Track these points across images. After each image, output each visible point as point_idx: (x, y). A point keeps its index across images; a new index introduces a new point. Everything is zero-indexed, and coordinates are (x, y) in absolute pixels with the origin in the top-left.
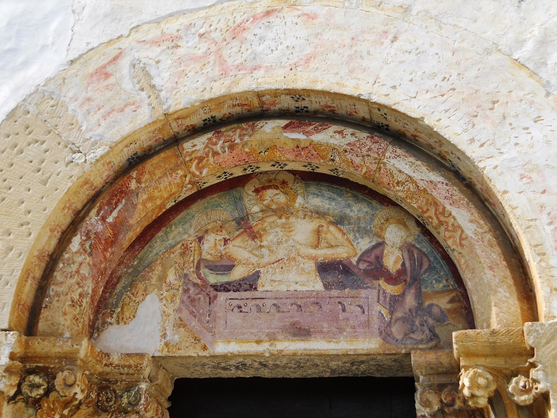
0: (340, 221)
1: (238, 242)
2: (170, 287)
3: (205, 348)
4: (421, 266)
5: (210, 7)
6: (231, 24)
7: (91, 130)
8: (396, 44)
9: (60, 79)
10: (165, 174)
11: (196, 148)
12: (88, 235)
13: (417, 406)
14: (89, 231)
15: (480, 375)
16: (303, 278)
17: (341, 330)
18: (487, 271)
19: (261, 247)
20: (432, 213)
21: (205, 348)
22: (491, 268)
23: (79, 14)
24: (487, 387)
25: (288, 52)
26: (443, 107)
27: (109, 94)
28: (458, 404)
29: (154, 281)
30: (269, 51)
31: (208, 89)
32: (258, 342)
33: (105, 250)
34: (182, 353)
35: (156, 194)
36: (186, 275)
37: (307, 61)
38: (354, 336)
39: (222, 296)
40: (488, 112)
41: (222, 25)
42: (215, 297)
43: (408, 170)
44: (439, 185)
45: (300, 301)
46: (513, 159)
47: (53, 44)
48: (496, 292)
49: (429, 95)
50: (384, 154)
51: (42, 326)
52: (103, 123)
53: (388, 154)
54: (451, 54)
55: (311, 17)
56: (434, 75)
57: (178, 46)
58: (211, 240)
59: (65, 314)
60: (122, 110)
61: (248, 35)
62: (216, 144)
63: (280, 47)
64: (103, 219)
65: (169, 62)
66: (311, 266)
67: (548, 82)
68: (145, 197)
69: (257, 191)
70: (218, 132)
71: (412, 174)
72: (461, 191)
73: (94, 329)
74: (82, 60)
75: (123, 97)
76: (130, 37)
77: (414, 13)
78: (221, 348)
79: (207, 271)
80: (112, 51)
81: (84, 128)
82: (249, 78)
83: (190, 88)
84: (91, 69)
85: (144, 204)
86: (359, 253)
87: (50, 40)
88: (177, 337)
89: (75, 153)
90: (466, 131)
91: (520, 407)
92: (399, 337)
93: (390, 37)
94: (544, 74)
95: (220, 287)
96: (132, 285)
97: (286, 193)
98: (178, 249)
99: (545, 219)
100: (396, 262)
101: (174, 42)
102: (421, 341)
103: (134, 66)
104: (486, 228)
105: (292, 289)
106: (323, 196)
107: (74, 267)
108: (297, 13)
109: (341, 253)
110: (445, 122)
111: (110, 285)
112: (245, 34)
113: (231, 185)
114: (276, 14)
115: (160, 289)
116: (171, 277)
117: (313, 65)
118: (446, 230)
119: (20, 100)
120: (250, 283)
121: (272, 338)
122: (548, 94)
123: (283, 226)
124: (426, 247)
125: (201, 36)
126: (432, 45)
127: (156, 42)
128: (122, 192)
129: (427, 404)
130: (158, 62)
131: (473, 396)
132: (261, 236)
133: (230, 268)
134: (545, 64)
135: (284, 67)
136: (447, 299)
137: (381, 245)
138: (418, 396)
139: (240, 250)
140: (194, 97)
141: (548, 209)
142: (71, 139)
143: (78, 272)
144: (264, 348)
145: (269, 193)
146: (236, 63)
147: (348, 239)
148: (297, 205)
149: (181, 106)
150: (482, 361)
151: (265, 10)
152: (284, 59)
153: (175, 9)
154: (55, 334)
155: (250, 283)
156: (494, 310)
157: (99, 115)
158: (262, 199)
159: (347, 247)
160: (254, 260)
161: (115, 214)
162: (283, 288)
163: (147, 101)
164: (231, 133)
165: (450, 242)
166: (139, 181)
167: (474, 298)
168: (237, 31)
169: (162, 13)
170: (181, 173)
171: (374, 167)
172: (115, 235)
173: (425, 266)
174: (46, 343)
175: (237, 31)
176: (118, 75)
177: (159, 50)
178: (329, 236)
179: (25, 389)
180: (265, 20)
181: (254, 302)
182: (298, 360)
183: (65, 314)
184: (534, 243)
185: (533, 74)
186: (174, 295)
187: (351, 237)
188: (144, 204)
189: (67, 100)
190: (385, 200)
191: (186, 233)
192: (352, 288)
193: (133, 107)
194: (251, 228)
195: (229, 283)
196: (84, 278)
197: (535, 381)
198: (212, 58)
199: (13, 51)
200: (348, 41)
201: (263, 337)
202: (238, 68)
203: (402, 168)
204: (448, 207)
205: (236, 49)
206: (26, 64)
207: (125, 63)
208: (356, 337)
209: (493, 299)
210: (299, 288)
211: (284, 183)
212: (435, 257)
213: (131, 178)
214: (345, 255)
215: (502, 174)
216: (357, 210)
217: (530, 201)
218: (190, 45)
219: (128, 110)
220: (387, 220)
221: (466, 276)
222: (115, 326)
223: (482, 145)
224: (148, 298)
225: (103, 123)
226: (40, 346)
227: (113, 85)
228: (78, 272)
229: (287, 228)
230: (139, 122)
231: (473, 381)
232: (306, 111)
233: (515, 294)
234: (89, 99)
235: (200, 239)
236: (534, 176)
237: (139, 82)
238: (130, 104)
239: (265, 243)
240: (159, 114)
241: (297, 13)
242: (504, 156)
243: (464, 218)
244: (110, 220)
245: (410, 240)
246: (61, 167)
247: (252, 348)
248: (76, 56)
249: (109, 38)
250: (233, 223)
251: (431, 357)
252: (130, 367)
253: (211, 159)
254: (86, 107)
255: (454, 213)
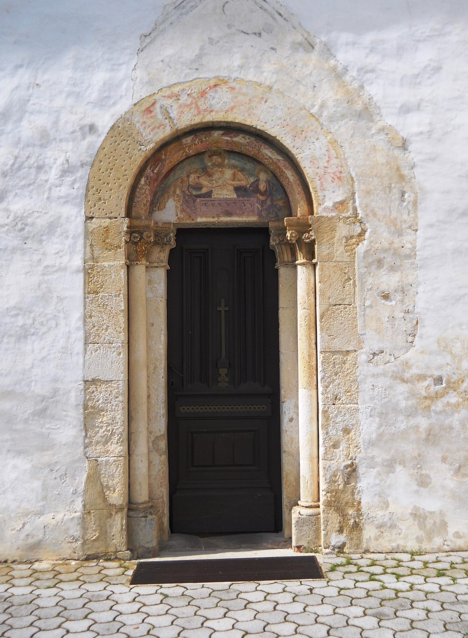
0: (242, 170)
1: (203, 178)
2: (178, 196)
3: (193, 220)
4: (273, 189)
5: (191, 81)
6: (200, 90)
7: (147, 136)
8: (267, 103)
9: (130, 112)
10: (176, 153)
11: (188, 142)
12: (147, 177)
13: (271, 241)
14: (148, 176)
15: (293, 233)
16: (229, 193)
17: (243, 213)
18: (297, 195)
19: (212, 180)
20: (278, 171)
21: (193, 220)
22: (298, 194)
23: (135, 81)
24: (296, 237)
25: (224, 105)
26: (284, 132)
27: (152, 120)
28: (285, 241)
29: (171, 193)
30: (216, 104)
31: (193, 120)
32: (213, 217)
33: (154, 183)
34: (184, 222)
35: (173, 160)
36: (184, 191)
37: (232, 109)
38: (248, 216)
39: (198, 200)
40: (300, 135)
41: (196, 90)
42: (196, 200)
43: (269, 154)
44: (281, 161)
45: (227, 201)
46: (308, 155)
47: (125, 95)
48: (300, 203)
49: (279, 127)
50: (260, 147)
51: (133, 214)
52: (151, 133)
53: (262, 148)
54: (287, 109)
55: (233, 89)
56: (280, 118)
57: (179, 99)
58: (192, 177)
59: (142, 209)
60: (159, 128)
61: (208, 96)
62: (195, 141)
63: (221, 102)
64: (153, 171)
65: (176, 106)
66: (231, 188)
67: (322, 124)
68: (168, 162)
69: (210, 157)
70: (196, 135)
71: (271, 156)
72: (289, 163)
73: (151, 212)
74: (139, 104)
75: (159, 122)
76: (159, 94)
77: (274, 90)
78: (199, 220)
79: (192, 189)
80: (151, 100)
81: (144, 135)
82: (209, 115)
83: (186, 120)
84: (144, 108)
85: (168, 164)
86: (250, 184)
87: (124, 94)
88: (182, 216)
89: (141, 145)
90: (292, 142)
91: (306, 243)
92: (265, 216)
93: (264, 100)
94: (321, 120)
95: (196, 197)
96: (162, 195)
97: (221, 158)
98: (180, 180)
99: (318, 178)
100: (264, 187)
101: (177, 97)
102: (272, 218)
103: (162, 108)
104: (297, 178)
105: (225, 197)
106: (235, 159)
107: (143, 191)
108: (227, 86)
109: (243, 183)
110: (284, 139)
111: (155, 195)
112: (207, 95)
113: (199, 154)
114: (218, 86)
115: (174, 196)
116: (178, 192)
117: (235, 111)
118: (283, 178)
119: (115, 121)
120: (209, 194)
121: (218, 216)
122: (322, 129)
123: (221, 172)
124: (275, 182)
125: (188, 95)
126: (280, 105)
127: (170, 97)
128: (159, 160)
129: (274, 240)
130: (171, 106)
131: (291, 240)
132: (212, 176)
133: (201, 188)
134: (322, 116)
135: (223, 111)
136: (282, 202)
137: (258, 180)
138: (271, 238)
139: (204, 181)
140: (188, 123)
141: (319, 175)
142: (139, 140)
143: (145, 193)
144: (215, 220)
145: (215, 158)
146: (204, 108)
147: (246, 178)
148: (226, 163)
149: (183, 127)
150: (294, 228)
151: (214, 84)
152: (223, 108)
153: (176, 81)
154: (138, 218)
155: (209, 194)
156: (299, 209)
157: (149, 130)
158: (212, 160)
159: (245, 181)
160: (210, 185)
161: (157, 169)
162: (222, 197)
163: (169, 124)
164: (201, 136)
165: (284, 183)
166: (165, 155)
167: (292, 204)
168: (203, 94)
169: (172, 82)
170: (182, 152)
171: (257, 152)
172: (157, 177)
173: (274, 189)
174: (138, 221)
175: (203, 94)
176: (155, 111)
177: (171, 101)
178: (238, 176)
179: (132, 239)
180: (214, 89)
181: (211, 202)
182: (227, 223)
183: (142, 209)
184: (314, 187)
185: (317, 120)
186: (180, 199)
187: (247, 177)
188: (168, 164)
189: (135, 122)
190: (259, 163)
191: (182, 174)
192: (247, 197)
193: (163, 127)
194: (208, 172)
195: (201, 194)
196: (147, 195)
197: (311, 236)
198: (193, 106)
199: (108, 97)
200: (248, 101)
201: (215, 216)
202: (205, 110)
203: (268, 152)
204: (284, 170)
205: (203, 102)
206: (115, 104)
207: (158, 106)
208: (249, 216)
209: (299, 205)
210: (228, 197)
211: (220, 153)
212: (278, 187)
213: (162, 154)
214: (245, 184)
215: (304, 160)
216: (249, 166)
217: (313, 171)
218: (184, 99)
219: (161, 128)
220: (260, 170)
221: (290, 195)
222: (157, 211)
223: (297, 149)
224: (170, 200)
225: (151, 133)
226: (136, 223)
227: (154, 116)
228: (145, 193)
229: (222, 173)
230: (166, 133)
231: (291, 234)
232: (230, 128)
233: (306, 203)
234: (144, 122)
235: (188, 176)
236: (315, 161)
237: (164, 115)
238: (161, 125)
239: (214, 178)
240: (174, 130)
241: (227, 86)
242: (305, 153)
243: (290, 174)
244: (155, 171)
245: (269, 178)
246: (136, 152)
247: (211, 220)
248: (136, 102)
249: (150, 94)
250: (201, 170)
251: (276, 224)
252: (166, 227)
253: (194, 146)
254: (144, 126)
255: (286, 172)
